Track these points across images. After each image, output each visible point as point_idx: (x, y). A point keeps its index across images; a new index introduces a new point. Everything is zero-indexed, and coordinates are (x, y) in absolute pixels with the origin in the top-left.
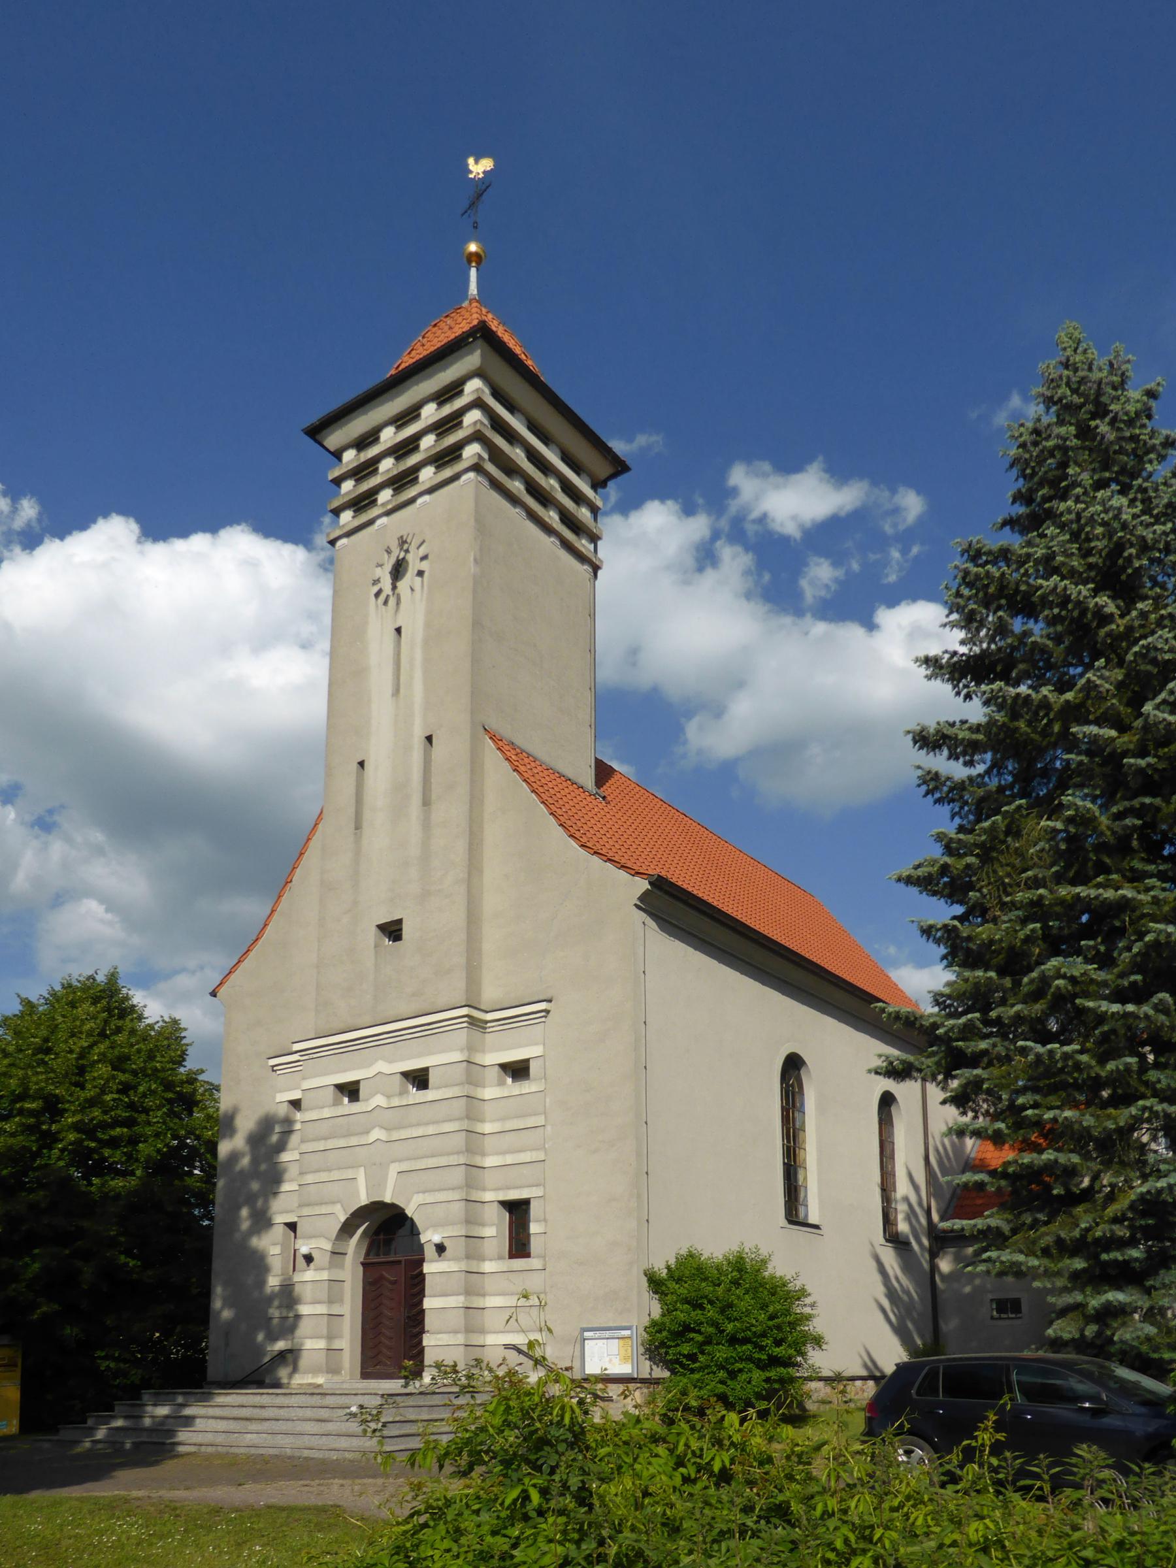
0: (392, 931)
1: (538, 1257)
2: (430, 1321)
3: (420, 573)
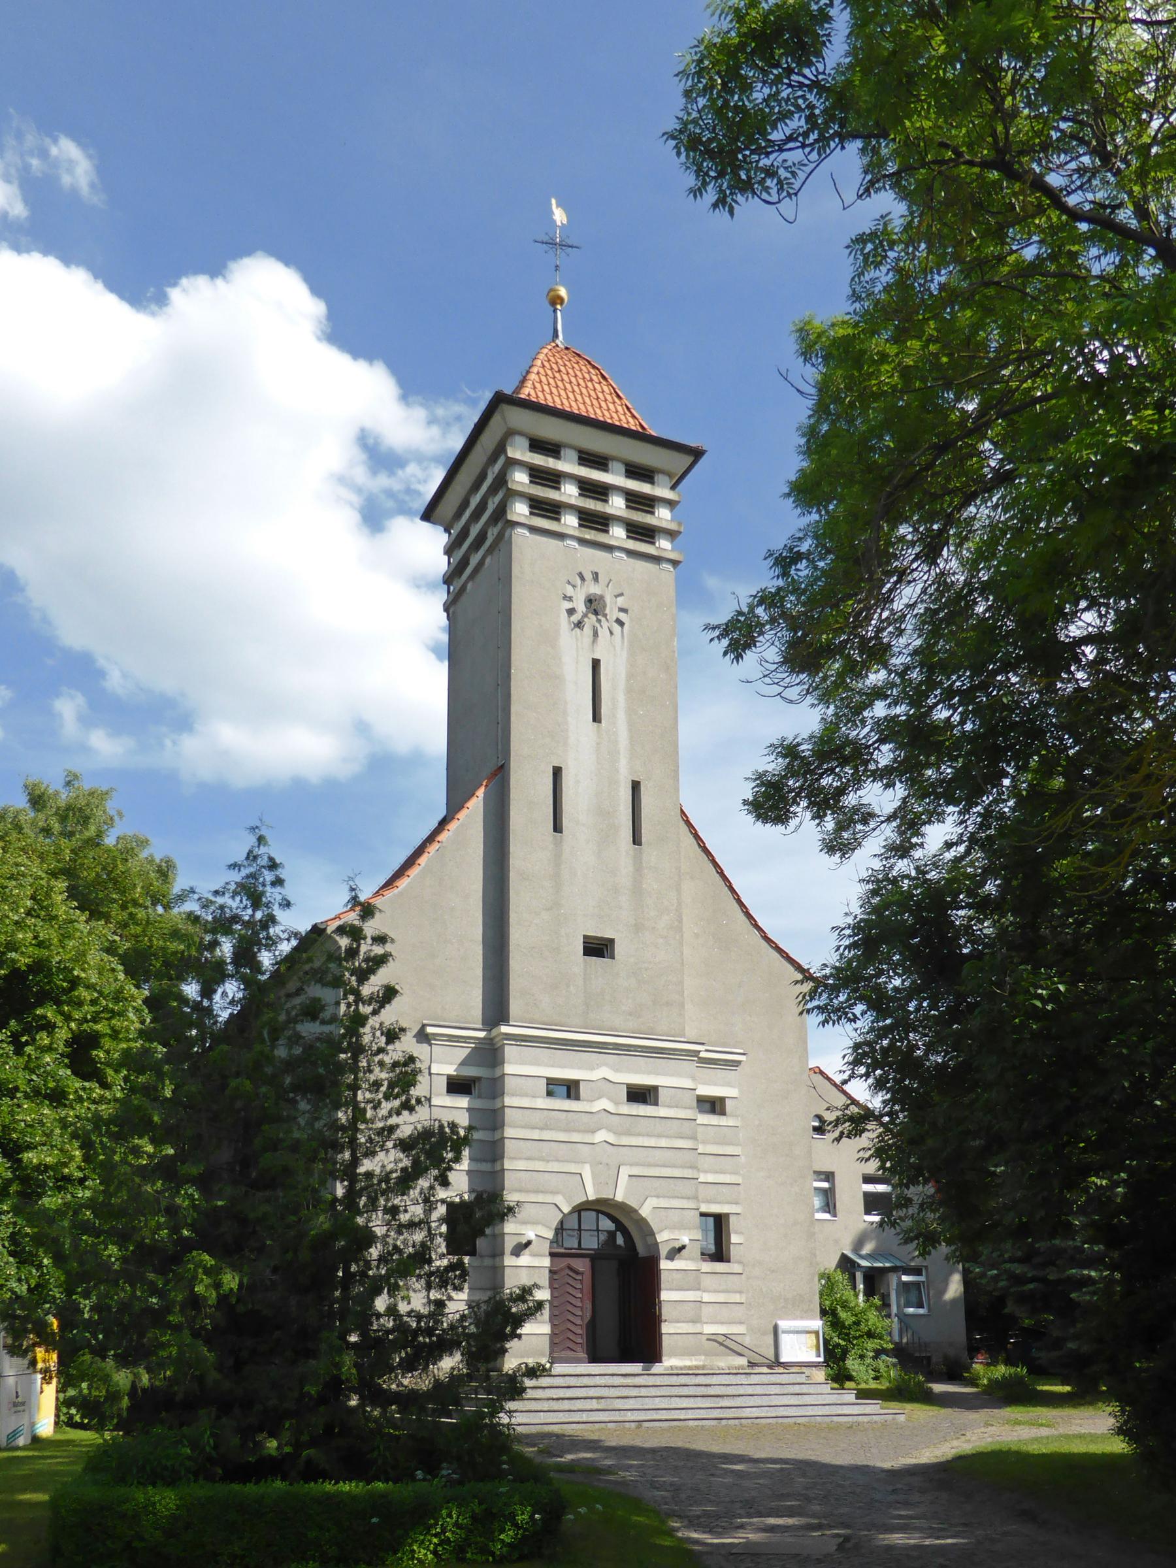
0: (598, 948)
1: (739, 1262)
2: (666, 1312)
3: (620, 623)
